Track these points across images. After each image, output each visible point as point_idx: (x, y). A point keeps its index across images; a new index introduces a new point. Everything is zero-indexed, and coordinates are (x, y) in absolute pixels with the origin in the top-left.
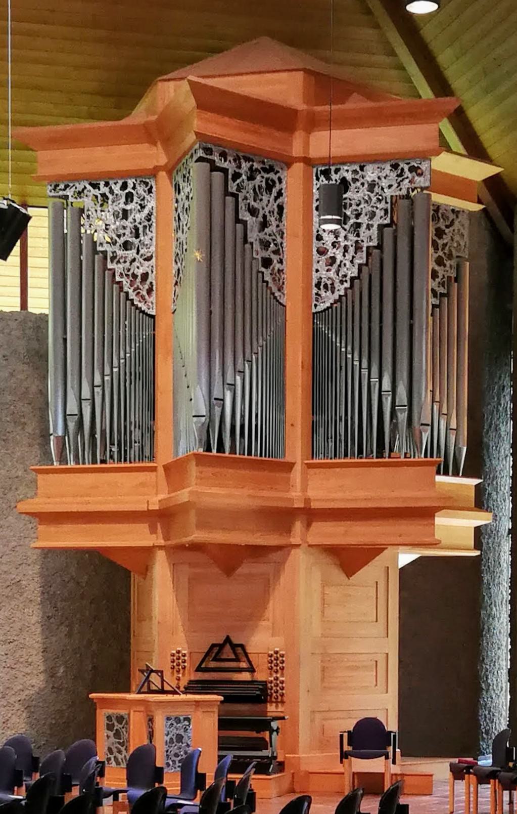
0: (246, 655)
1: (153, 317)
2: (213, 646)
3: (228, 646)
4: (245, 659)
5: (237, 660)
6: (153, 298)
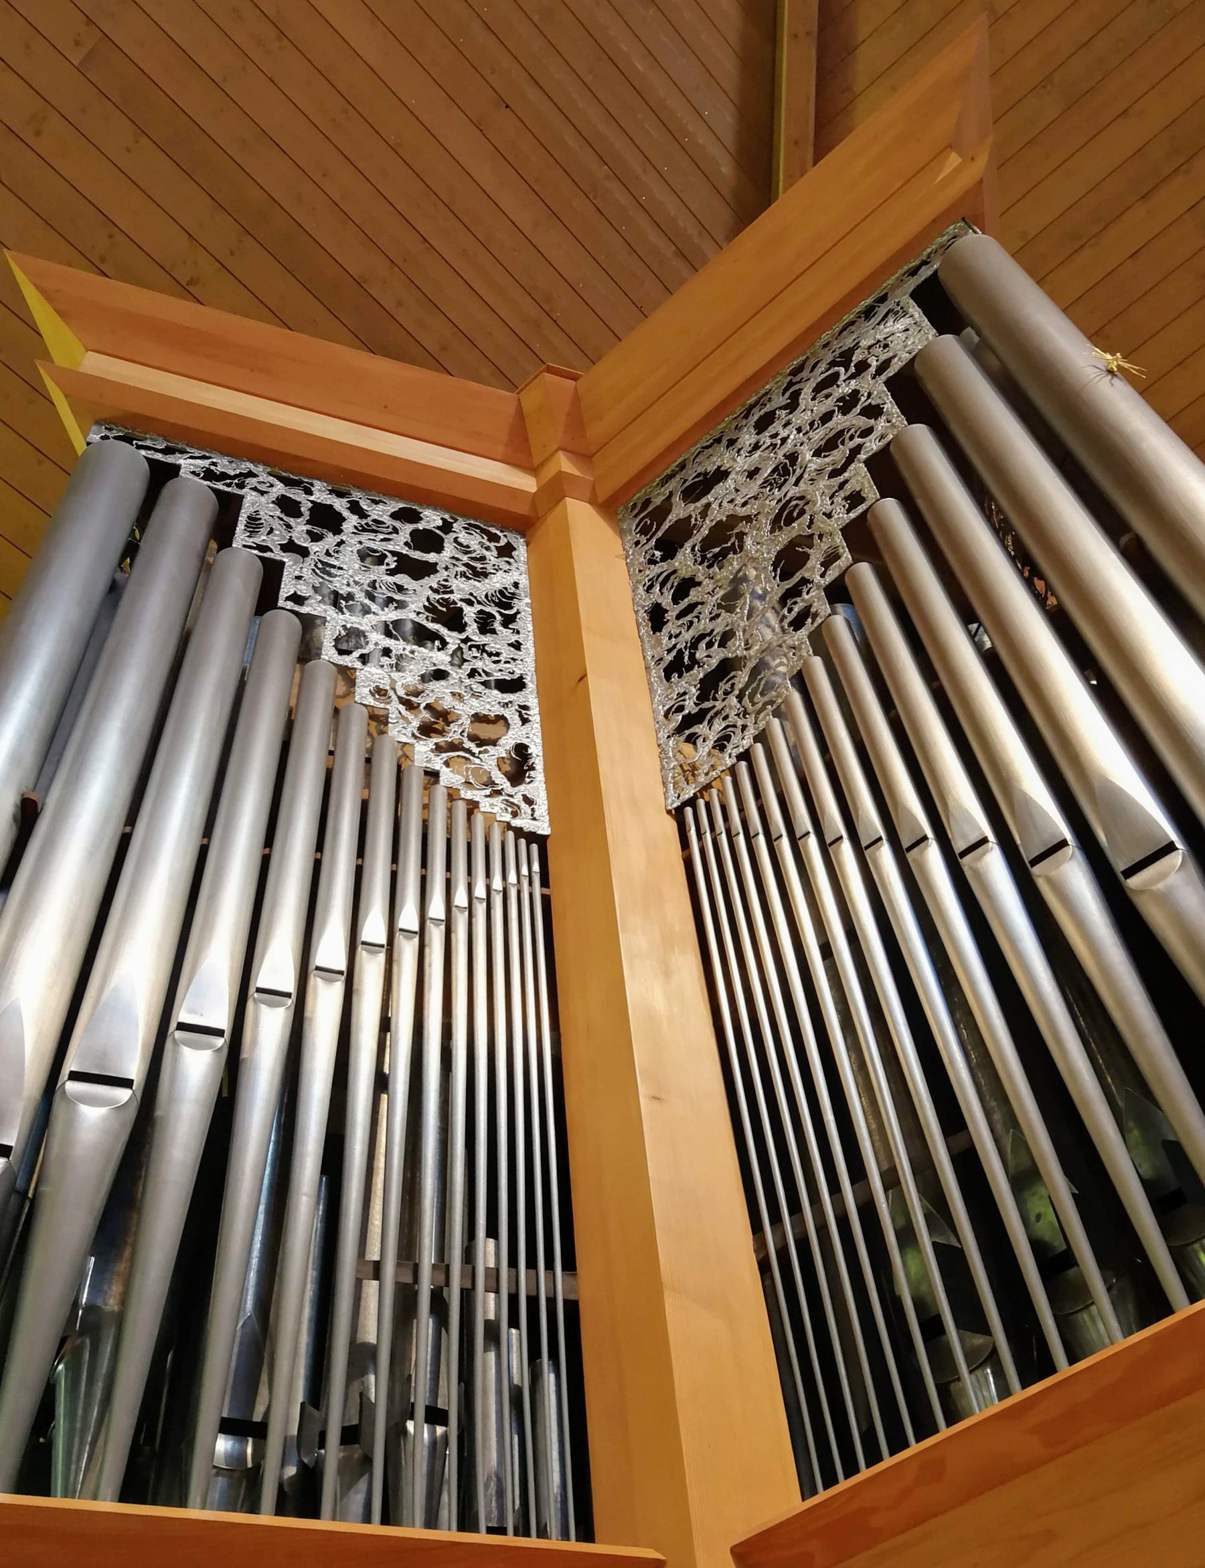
1: (541, 841)
6: (537, 786)
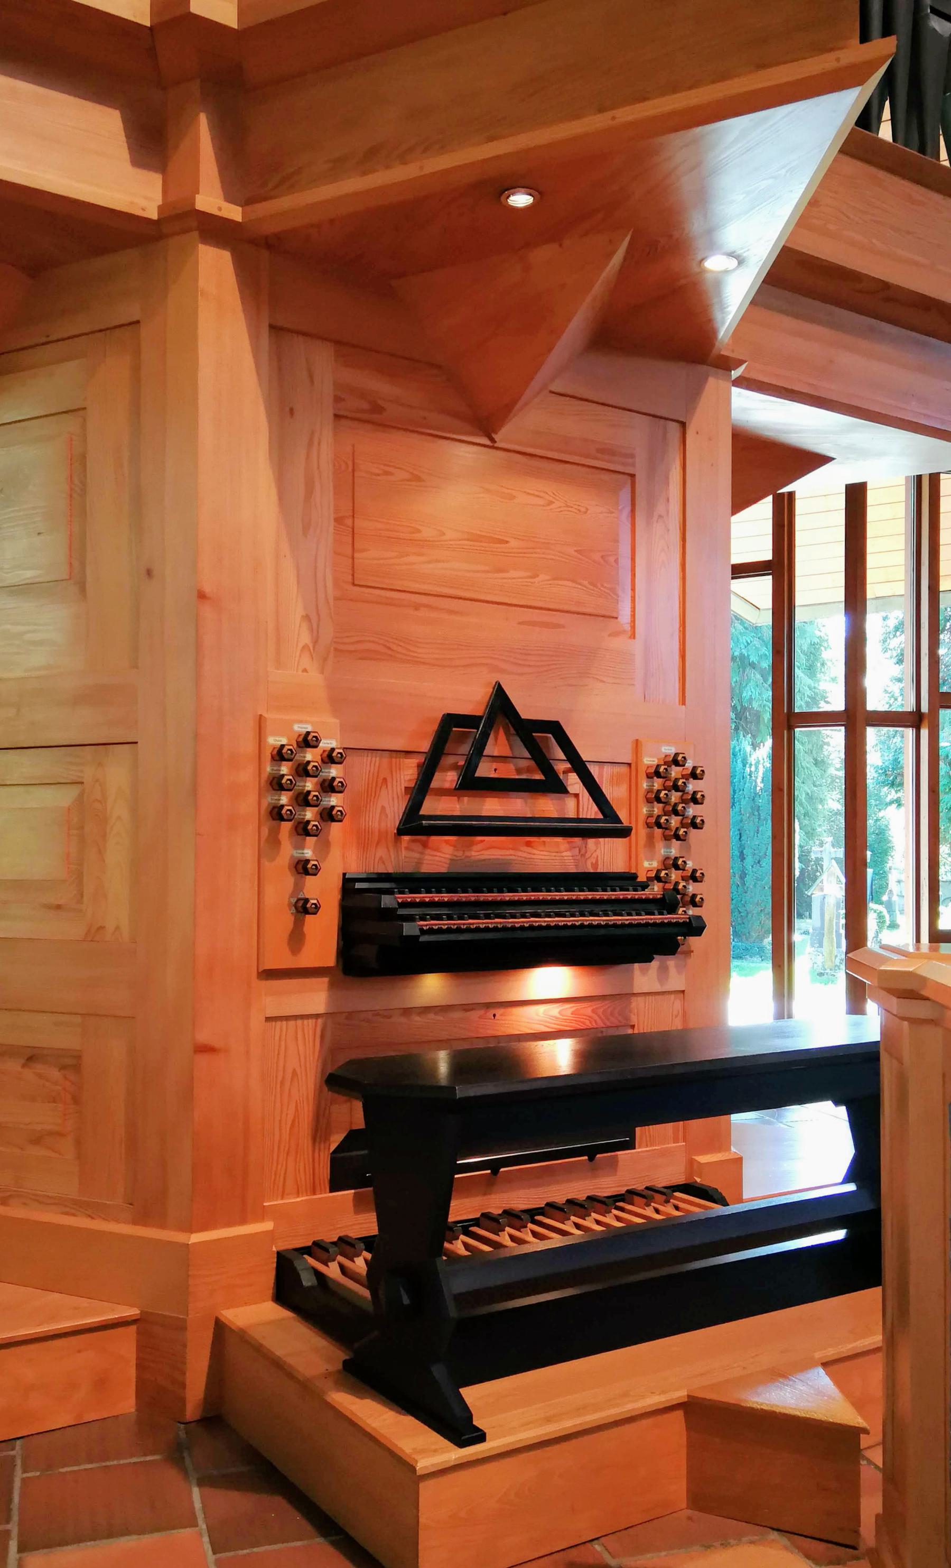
0: (579, 766)
2: (451, 722)
3: (496, 745)
4: (574, 782)
5: (554, 786)
